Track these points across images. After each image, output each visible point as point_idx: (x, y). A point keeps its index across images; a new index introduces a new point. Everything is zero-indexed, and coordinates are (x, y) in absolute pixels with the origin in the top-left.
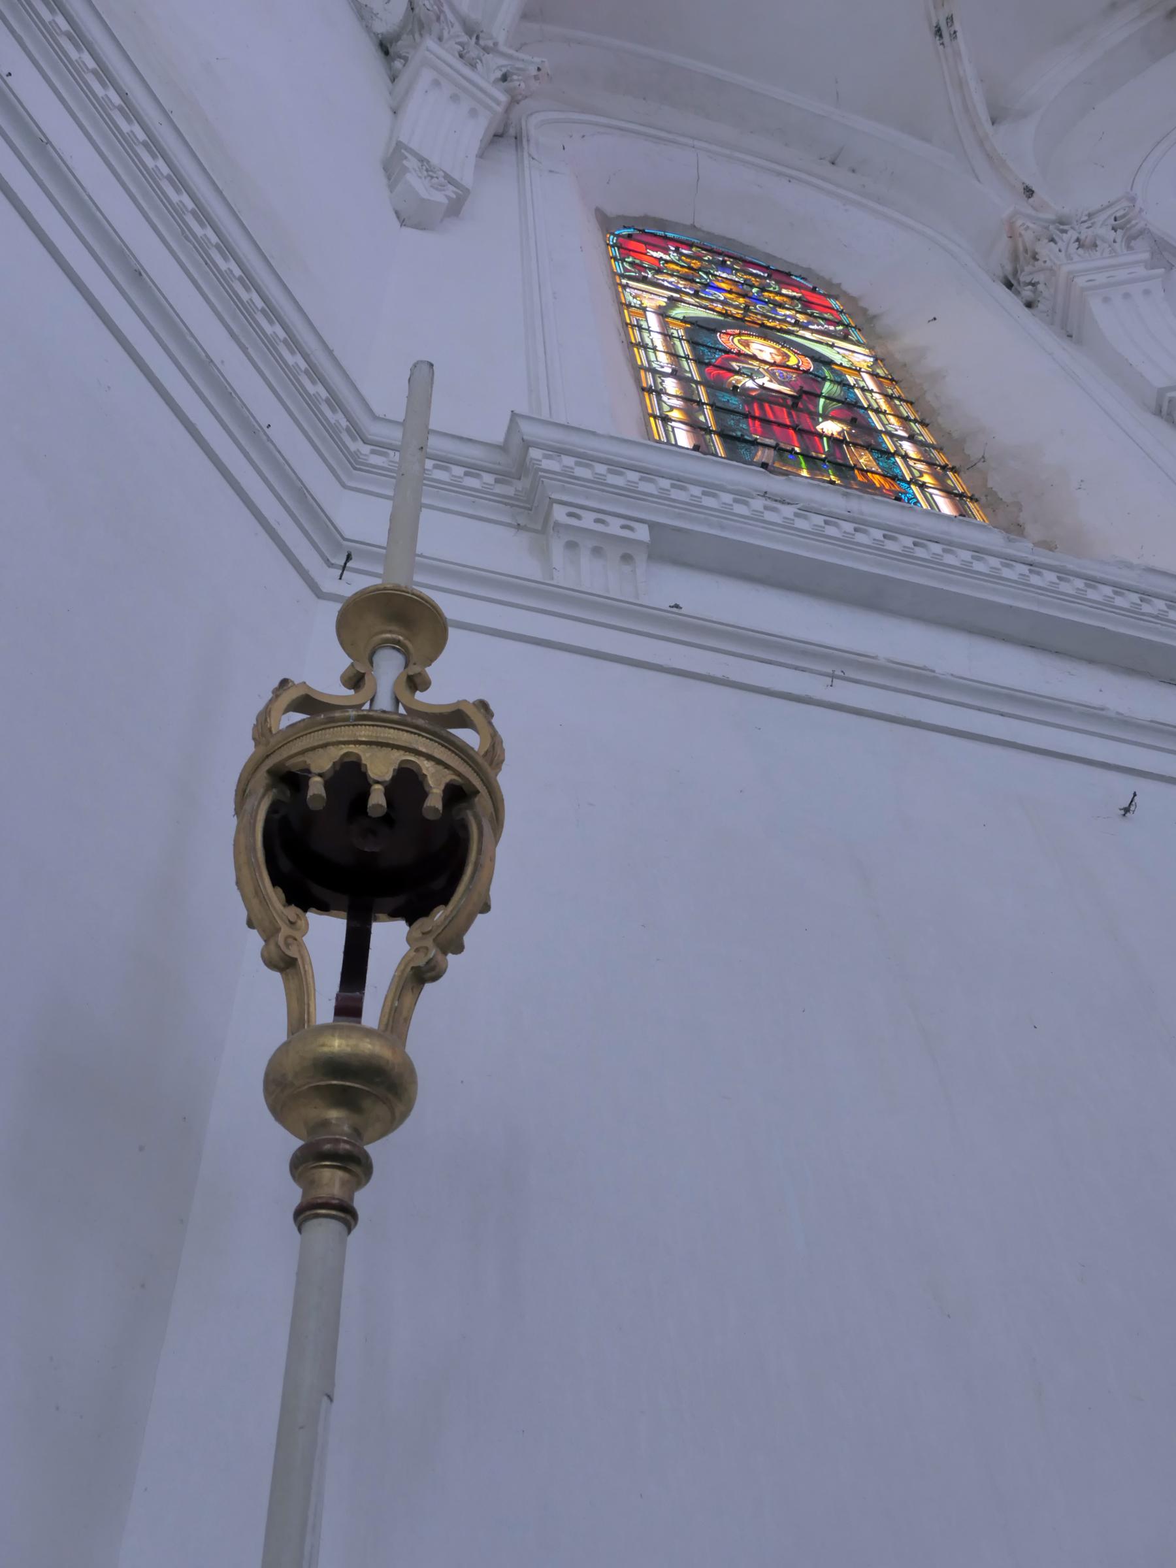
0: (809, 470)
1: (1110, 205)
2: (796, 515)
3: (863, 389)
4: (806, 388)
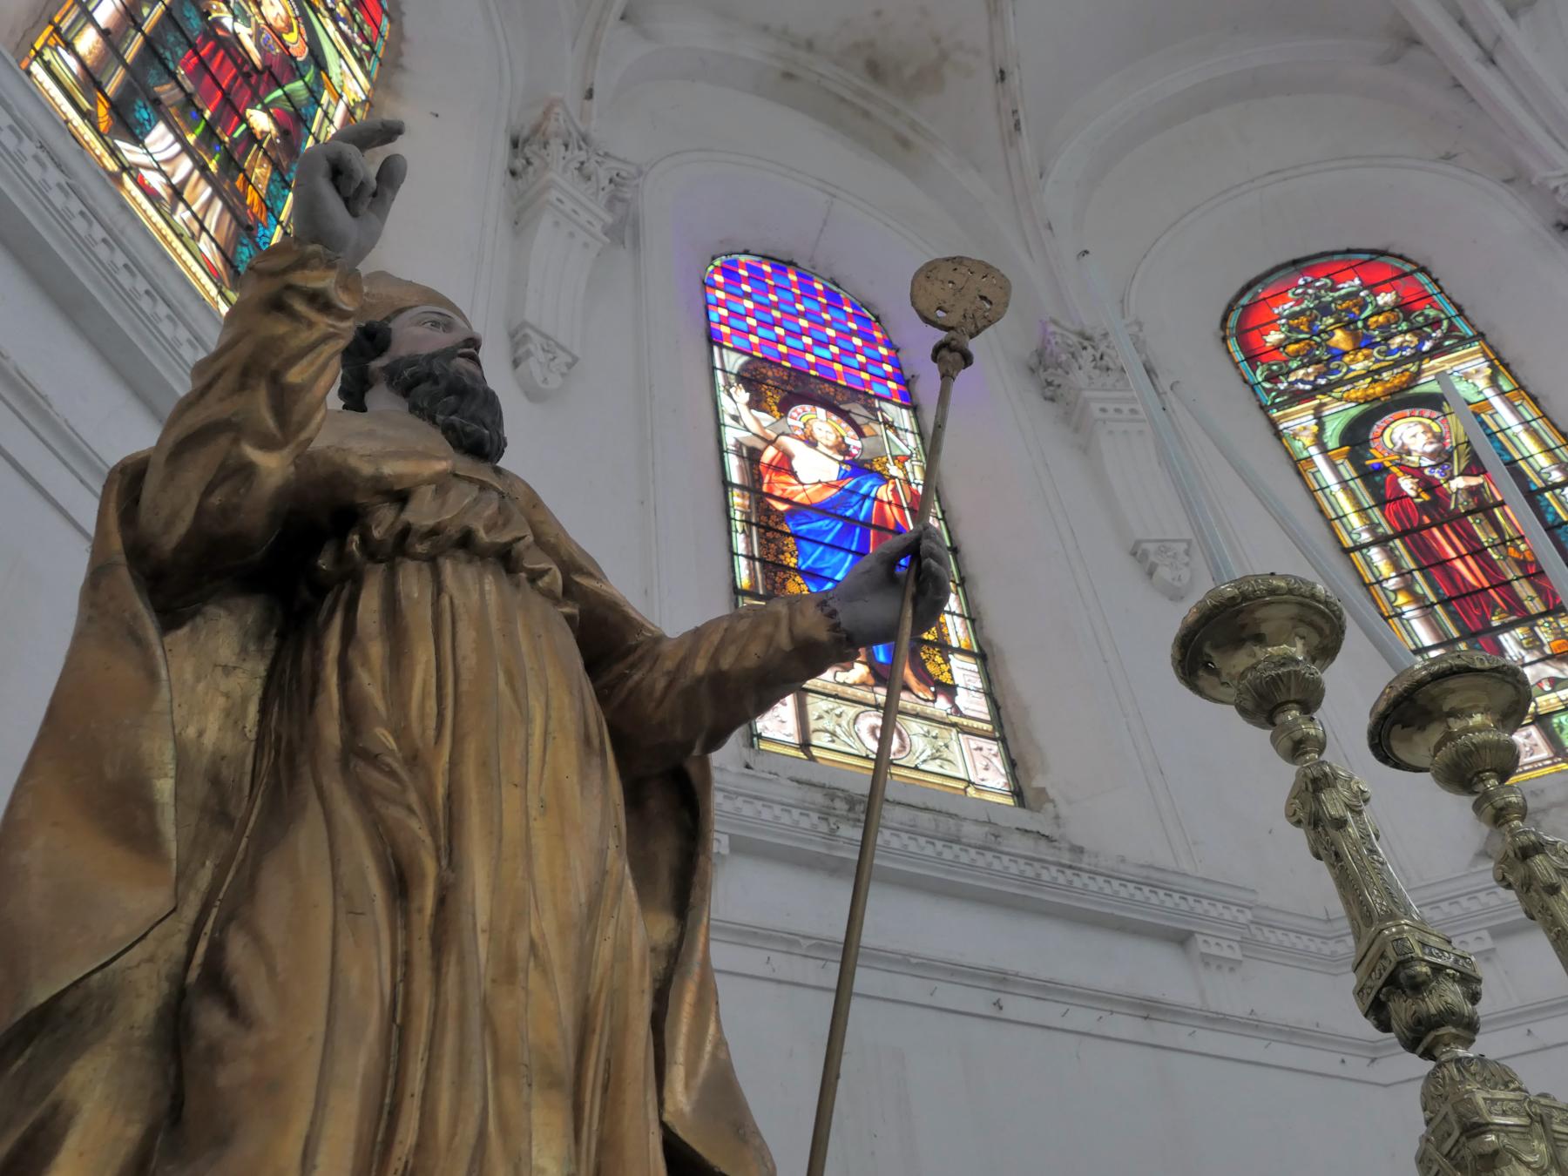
0: (200, 139)
1: (624, 161)
2: (59, 185)
3: (326, 114)
4: (275, 70)
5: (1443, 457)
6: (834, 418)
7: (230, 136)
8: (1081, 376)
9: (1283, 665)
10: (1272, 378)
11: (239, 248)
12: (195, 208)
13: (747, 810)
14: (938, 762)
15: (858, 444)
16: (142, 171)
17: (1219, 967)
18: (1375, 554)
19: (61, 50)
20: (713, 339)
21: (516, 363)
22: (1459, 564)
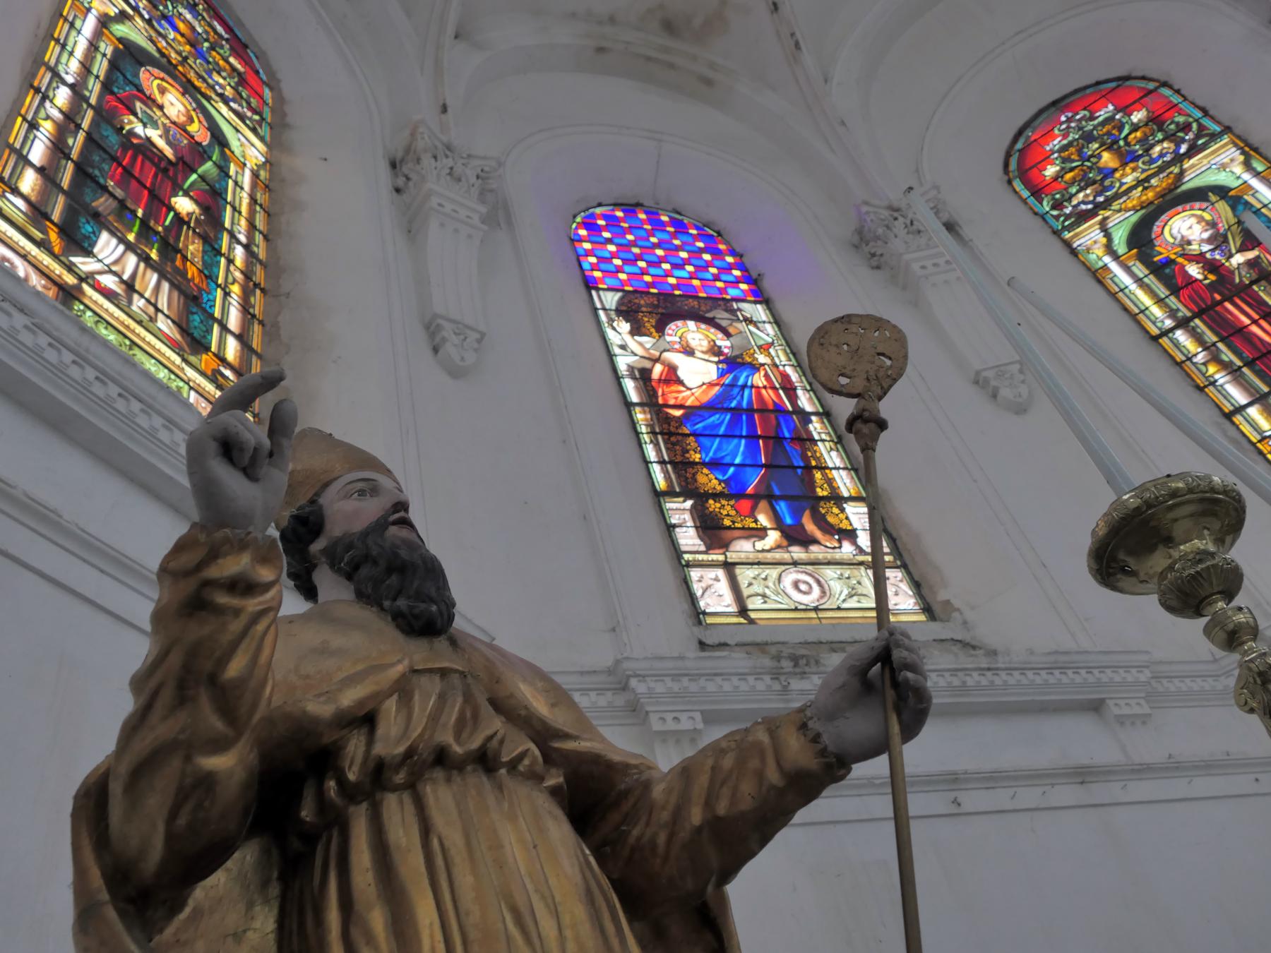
0: (138, 235)
1: (485, 158)
2: (26, 327)
3: (236, 183)
4: (188, 159)
5: (1219, 240)
6: (703, 326)
7: (162, 225)
8: (898, 243)
9: (1200, 561)
10: (1057, 205)
11: (191, 317)
12: (147, 295)
13: (711, 687)
14: (855, 598)
15: (728, 343)
16: (98, 277)
17: (1133, 723)
18: (1180, 335)
19: (8, 195)
20: (590, 285)
21: (436, 350)
22: (1254, 329)
